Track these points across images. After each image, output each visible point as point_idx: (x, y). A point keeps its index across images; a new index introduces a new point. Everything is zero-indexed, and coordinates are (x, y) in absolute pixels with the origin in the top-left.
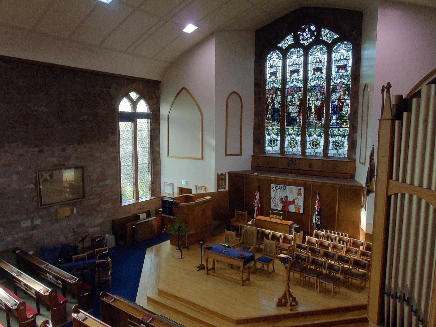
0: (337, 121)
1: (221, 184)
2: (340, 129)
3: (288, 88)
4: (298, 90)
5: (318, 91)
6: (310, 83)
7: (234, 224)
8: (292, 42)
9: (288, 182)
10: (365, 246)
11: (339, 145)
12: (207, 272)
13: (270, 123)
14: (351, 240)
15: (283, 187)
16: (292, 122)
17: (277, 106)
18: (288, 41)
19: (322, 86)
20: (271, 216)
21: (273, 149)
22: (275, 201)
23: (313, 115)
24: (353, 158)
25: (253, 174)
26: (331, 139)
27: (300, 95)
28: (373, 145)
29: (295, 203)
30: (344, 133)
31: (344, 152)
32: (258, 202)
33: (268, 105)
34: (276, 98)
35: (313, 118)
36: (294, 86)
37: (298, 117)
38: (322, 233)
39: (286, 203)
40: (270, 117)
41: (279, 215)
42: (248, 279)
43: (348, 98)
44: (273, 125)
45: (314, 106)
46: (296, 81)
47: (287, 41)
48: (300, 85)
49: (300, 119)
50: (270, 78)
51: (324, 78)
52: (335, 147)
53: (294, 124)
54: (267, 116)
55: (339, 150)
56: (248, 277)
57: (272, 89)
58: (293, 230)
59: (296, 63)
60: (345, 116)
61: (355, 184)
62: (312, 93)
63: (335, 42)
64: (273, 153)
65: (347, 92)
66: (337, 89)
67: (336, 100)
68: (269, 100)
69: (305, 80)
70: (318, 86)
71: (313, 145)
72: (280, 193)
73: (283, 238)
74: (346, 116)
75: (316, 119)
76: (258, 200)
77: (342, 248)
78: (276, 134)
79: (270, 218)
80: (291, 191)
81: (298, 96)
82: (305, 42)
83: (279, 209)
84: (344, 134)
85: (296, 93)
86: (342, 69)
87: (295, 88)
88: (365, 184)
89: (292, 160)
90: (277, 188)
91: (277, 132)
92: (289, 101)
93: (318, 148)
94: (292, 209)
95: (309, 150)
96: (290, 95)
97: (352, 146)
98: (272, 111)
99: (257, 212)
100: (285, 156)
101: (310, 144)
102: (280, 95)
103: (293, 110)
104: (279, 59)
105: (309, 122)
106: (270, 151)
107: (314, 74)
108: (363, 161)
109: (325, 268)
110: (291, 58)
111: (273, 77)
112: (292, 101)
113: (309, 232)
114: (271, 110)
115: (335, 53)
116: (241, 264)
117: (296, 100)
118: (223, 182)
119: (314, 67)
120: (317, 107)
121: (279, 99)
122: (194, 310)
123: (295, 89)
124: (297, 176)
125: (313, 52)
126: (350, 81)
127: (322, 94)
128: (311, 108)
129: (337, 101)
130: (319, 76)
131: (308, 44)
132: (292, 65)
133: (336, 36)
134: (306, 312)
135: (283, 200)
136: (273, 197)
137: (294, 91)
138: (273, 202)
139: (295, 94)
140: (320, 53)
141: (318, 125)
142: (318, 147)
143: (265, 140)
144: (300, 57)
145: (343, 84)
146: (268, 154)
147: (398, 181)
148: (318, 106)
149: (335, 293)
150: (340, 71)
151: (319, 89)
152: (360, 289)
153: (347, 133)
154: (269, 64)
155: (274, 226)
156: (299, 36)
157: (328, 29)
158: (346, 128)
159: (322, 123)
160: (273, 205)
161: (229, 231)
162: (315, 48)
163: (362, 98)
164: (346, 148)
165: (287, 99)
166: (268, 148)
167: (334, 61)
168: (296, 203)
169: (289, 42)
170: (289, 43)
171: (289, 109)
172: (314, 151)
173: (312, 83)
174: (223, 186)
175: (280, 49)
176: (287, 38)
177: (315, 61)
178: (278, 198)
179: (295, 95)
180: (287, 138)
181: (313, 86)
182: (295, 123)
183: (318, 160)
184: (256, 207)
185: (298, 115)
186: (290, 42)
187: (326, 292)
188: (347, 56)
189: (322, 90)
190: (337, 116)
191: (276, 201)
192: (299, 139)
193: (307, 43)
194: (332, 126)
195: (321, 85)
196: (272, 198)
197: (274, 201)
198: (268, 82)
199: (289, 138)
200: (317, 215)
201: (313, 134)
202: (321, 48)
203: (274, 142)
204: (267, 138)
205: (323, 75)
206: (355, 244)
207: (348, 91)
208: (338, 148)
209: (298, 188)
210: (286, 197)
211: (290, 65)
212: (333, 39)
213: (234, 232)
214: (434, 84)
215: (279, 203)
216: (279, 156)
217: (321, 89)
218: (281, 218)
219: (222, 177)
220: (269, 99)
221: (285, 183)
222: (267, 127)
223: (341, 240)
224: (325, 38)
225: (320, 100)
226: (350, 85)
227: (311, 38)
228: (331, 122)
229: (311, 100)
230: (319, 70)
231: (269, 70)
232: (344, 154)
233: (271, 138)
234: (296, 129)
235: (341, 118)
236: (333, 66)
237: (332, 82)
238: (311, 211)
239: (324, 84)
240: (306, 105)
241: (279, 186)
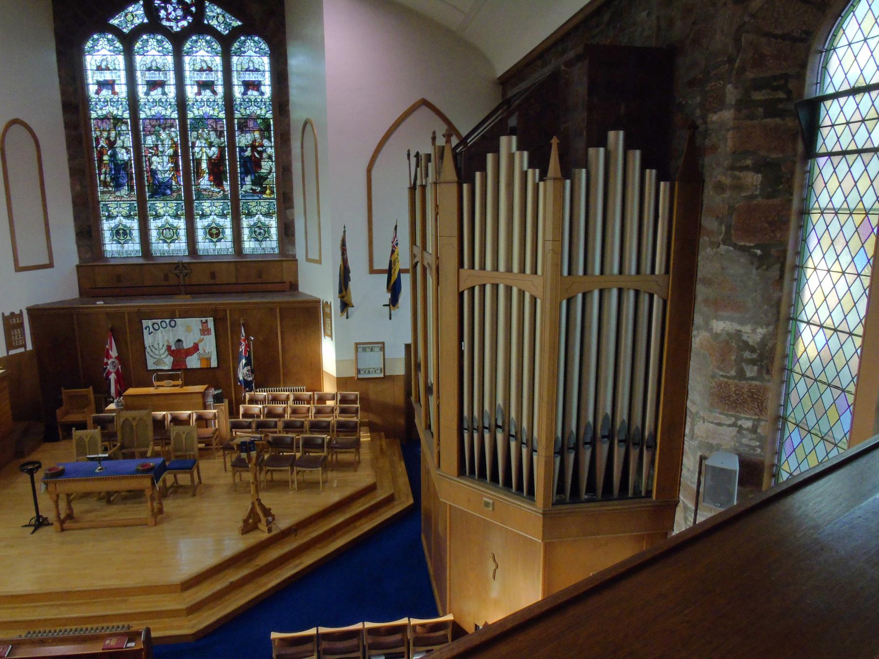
0: (254, 188)
1: (13, 337)
2: (260, 202)
3: (145, 119)
4: (167, 125)
5: (211, 128)
6: (192, 111)
7: (63, 420)
8: (143, 20)
9: (179, 311)
10: (338, 399)
11: (262, 231)
12: (61, 525)
13: (109, 192)
14: (314, 394)
15: (170, 322)
16: (160, 190)
17: (123, 155)
18: (132, 15)
19: (218, 119)
20: (156, 383)
21: (217, 247)
22: (155, 354)
23: (206, 176)
24: (291, 253)
25: (95, 306)
26: (245, 222)
27: (173, 134)
28: (345, 227)
29: (198, 350)
30: (269, 209)
31: (272, 244)
32: (117, 362)
33: (101, 154)
34: (118, 138)
35: (205, 182)
36: (158, 116)
37: (175, 181)
38: (261, 394)
39: (179, 353)
40: (108, 179)
41: (172, 378)
42: (161, 511)
43: (270, 145)
44: (118, 196)
45: (204, 157)
46: (160, 106)
47: (130, 15)
48: (171, 114)
49: (177, 183)
50: (97, 93)
51: (220, 103)
52: (253, 235)
53: (164, 194)
54: (100, 177)
55: (262, 241)
56: (160, 507)
57: (104, 118)
58: (210, 400)
59: (157, 67)
60: (267, 178)
61: (300, 299)
62: (198, 131)
63: (235, 34)
64: (125, 256)
65: (266, 134)
66: (246, 126)
67: (247, 147)
68: (103, 143)
69: (182, 104)
70: (210, 118)
71: (211, 235)
72: (163, 336)
73: (196, 420)
74: (269, 177)
75: (212, 183)
76: (116, 358)
77: (308, 409)
78: (128, 217)
79: (156, 388)
80: (188, 329)
81: (169, 137)
82: (172, 24)
83: (166, 368)
84: (269, 211)
85: (164, 129)
86: (253, 89)
87: (159, 119)
88: (338, 293)
89: (178, 266)
90: (156, 327)
91: (130, 212)
92: (149, 146)
93: (223, 240)
94: (193, 362)
95: (204, 244)
96: (151, 134)
97: (287, 231)
98: (113, 167)
99: (116, 383)
100: (107, 262)
101: (205, 233)
102: (127, 132)
103: (161, 165)
104: (117, 54)
105: (198, 190)
106: (119, 252)
107: (199, 93)
108: (314, 255)
109: (299, 447)
110: (143, 55)
111: (106, 93)
112: (157, 146)
113: (234, 400)
114: (109, 164)
115: (237, 56)
116: (146, 482)
117: (167, 146)
118: (19, 332)
119: (196, 79)
120: (213, 161)
121: (126, 142)
122: (72, 605)
123: (162, 121)
124: (194, 298)
125: (192, 47)
126: (271, 112)
127: (220, 135)
128: (198, 162)
129: (249, 149)
130: (209, 99)
131: (178, 29)
132: (149, 69)
133: (237, 23)
134: (293, 526)
135: (173, 348)
136: (149, 346)
137: (159, 126)
138: (151, 356)
139: (161, 132)
140: (207, 52)
141: (216, 194)
142: (222, 238)
143: (102, 230)
144: (165, 55)
145: (258, 117)
146: (112, 260)
147: (497, 270)
148: (213, 157)
149: (325, 482)
150: (250, 92)
151: (212, 124)
152: (353, 466)
153: (274, 208)
154: (91, 62)
155: (167, 402)
156: (158, 10)
157: (219, 6)
158: (271, 201)
159: (224, 191)
160: (152, 362)
161: (82, 431)
162: (196, 41)
163: (299, 144)
164: (275, 237)
165: (145, 142)
166: (110, 247)
167: (237, 71)
168: (201, 351)
169: (136, 19)
170: (137, 21)
171: (152, 163)
172: (214, 247)
173: (196, 112)
174: (20, 341)
175: (116, 31)
176: (130, 9)
177: (198, 67)
178: (161, 346)
179: (163, 135)
180: (154, 224)
181: (198, 117)
182: (168, 192)
183: (226, 262)
184: (111, 373)
185: (173, 175)
186: (138, 19)
187: (311, 486)
188: (260, 64)
189: (218, 126)
190: (253, 178)
191: (157, 352)
192: (181, 224)
193: (178, 27)
194: (244, 196)
195: (214, 117)
196: (148, 349)
197: (152, 354)
198: (93, 103)
199: (159, 223)
200: (246, 365)
201: (209, 213)
202: (208, 42)
203: (125, 233)
204: (107, 225)
205: (218, 97)
206: (322, 399)
207: (269, 130)
208: (260, 238)
209: (202, 321)
210: (179, 341)
211: (145, 69)
212: (231, 27)
213: (96, 430)
214: (602, 147)
215: (165, 355)
216: (141, 261)
217: (216, 126)
218: (180, 382)
219: (14, 319)
220: (101, 141)
221: (172, 315)
222: (104, 203)
223: (297, 400)
224: (214, 23)
225: (216, 146)
226: (271, 120)
227: (184, 18)
228: (241, 188)
229: (197, 145)
230: (204, 85)
231: (92, 78)
232: (273, 249)
233: (117, 226)
234: (173, 204)
235: (259, 181)
236: (235, 81)
237: (236, 112)
238: (233, 362)
239: (222, 115)
240: (188, 155)
241: (162, 322)
